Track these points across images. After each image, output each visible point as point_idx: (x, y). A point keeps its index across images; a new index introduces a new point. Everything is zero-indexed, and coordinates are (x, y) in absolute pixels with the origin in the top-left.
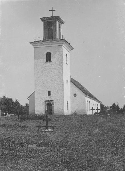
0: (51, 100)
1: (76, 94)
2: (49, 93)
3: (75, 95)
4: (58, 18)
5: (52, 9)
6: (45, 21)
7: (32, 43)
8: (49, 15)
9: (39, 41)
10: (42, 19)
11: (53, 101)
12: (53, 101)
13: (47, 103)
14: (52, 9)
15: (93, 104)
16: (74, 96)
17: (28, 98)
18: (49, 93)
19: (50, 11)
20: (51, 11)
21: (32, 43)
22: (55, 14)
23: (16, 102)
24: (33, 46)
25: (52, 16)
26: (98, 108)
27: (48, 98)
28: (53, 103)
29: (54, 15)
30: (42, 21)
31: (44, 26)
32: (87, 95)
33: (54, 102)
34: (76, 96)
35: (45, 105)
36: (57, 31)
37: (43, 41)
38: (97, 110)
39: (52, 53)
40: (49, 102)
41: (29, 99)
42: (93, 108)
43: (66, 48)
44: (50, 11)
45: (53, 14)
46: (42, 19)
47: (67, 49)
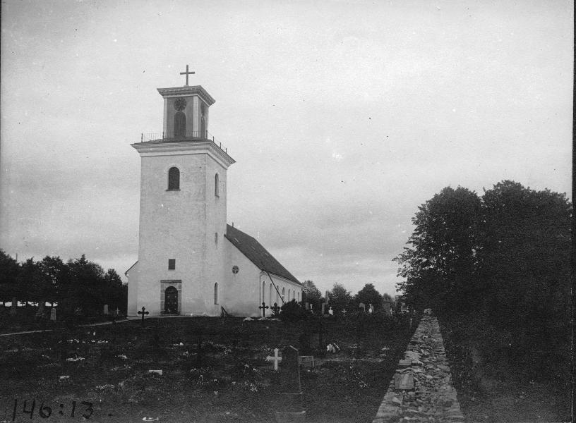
1: (239, 267)
2: (172, 264)
3: (235, 270)
5: (187, 84)
6: (169, 97)
7: (135, 146)
8: (179, 82)
10: (163, 92)
11: (180, 281)
12: (180, 281)
13: (167, 286)
14: (187, 84)
15: (292, 292)
16: (234, 272)
17: (126, 274)
18: (172, 264)
20: (189, 71)
21: (135, 146)
24: (139, 152)
26: (147, 313)
27: (171, 275)
28: (180, 287)
29: (190, 84)
30: (163, 95)
31: (166, 109)
32: (263, 270)
33: (183, 285)
34: (237, 272)
35: (161, 291)
37: (163, 141)
38: (262, 309)
39: (181, 171)
40: (171, 285)
41: (128, 275)
42: (264, 304)
43: (221, 162)
46: (163, 92)
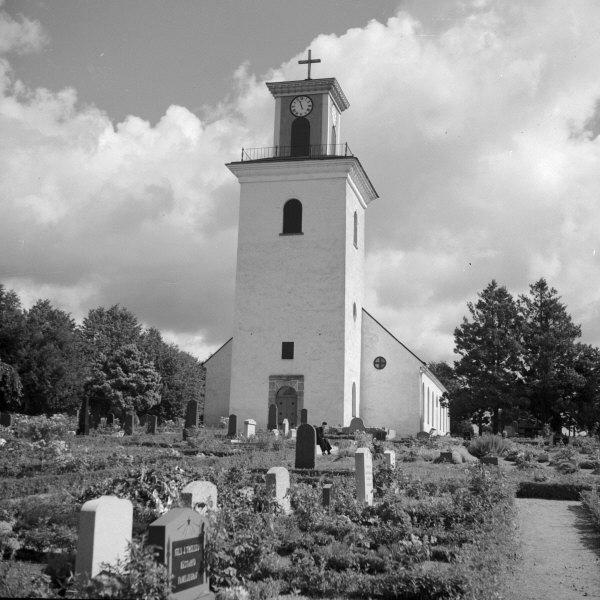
0: (294, 373)
2: (288, 351)
3: (380, 363)
4: (329, 84)
9: (251, 162)
11: (300, 377)
13: (279, 385)
18: (288, 351)
19: (319, 61)
22: (318, 72)
23: (251, 75)
25: (309, 79)
27: (287, 368)
28: (302, 386)
29: (314, 77)
36: (326, 134)
44: (319, 61)
45: (312, 73)
46: (302, 234)
47: (358, 197)
